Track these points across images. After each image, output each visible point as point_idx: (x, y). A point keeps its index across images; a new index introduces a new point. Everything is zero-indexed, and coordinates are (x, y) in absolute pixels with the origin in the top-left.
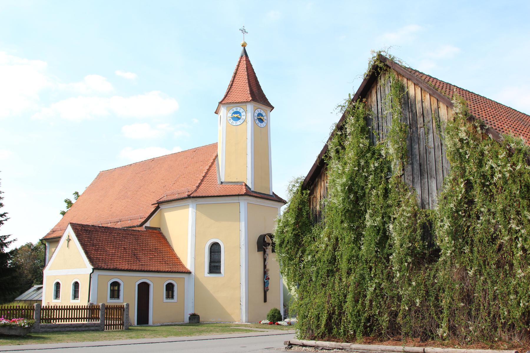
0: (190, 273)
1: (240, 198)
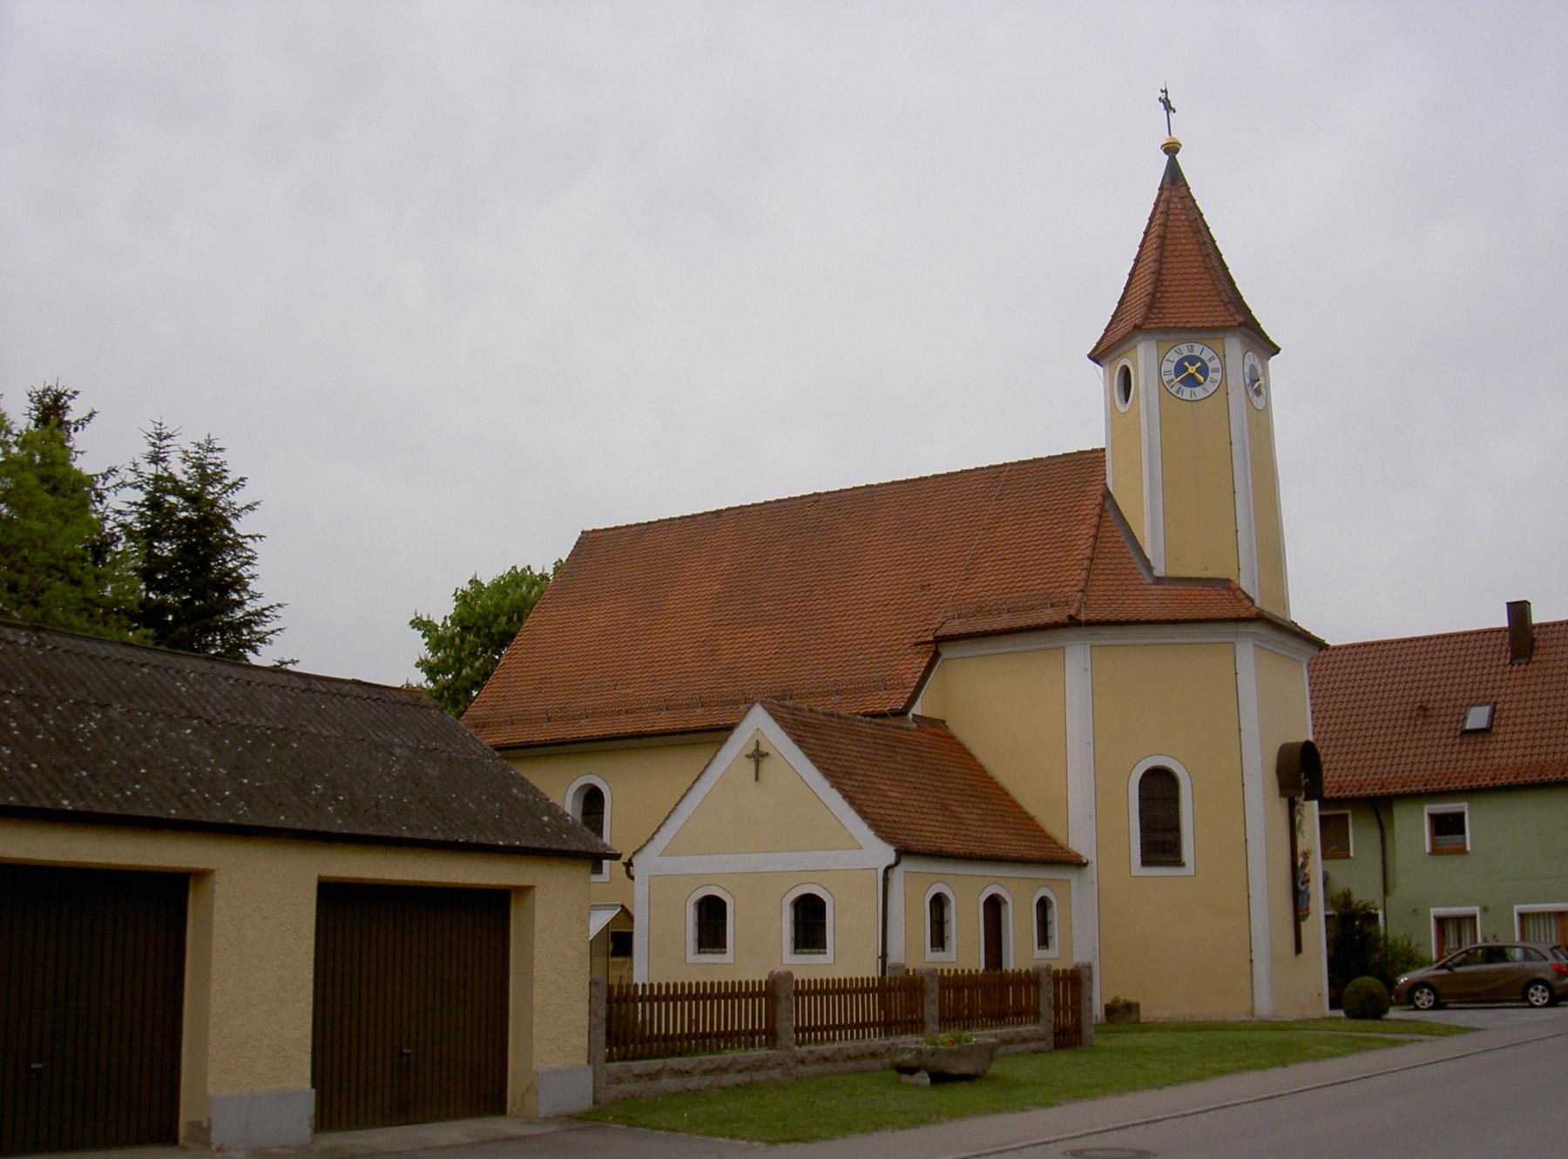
0: (1078, 864)
1: (1242, 628)
